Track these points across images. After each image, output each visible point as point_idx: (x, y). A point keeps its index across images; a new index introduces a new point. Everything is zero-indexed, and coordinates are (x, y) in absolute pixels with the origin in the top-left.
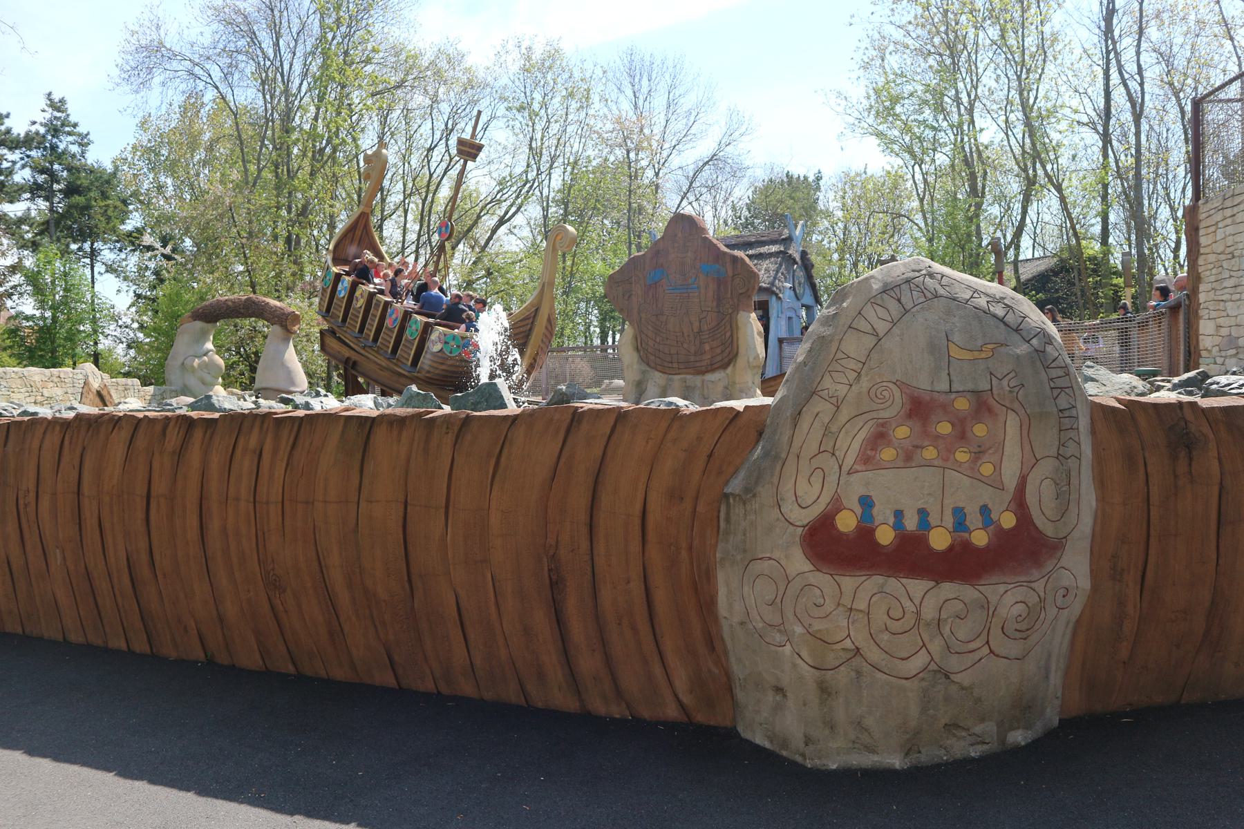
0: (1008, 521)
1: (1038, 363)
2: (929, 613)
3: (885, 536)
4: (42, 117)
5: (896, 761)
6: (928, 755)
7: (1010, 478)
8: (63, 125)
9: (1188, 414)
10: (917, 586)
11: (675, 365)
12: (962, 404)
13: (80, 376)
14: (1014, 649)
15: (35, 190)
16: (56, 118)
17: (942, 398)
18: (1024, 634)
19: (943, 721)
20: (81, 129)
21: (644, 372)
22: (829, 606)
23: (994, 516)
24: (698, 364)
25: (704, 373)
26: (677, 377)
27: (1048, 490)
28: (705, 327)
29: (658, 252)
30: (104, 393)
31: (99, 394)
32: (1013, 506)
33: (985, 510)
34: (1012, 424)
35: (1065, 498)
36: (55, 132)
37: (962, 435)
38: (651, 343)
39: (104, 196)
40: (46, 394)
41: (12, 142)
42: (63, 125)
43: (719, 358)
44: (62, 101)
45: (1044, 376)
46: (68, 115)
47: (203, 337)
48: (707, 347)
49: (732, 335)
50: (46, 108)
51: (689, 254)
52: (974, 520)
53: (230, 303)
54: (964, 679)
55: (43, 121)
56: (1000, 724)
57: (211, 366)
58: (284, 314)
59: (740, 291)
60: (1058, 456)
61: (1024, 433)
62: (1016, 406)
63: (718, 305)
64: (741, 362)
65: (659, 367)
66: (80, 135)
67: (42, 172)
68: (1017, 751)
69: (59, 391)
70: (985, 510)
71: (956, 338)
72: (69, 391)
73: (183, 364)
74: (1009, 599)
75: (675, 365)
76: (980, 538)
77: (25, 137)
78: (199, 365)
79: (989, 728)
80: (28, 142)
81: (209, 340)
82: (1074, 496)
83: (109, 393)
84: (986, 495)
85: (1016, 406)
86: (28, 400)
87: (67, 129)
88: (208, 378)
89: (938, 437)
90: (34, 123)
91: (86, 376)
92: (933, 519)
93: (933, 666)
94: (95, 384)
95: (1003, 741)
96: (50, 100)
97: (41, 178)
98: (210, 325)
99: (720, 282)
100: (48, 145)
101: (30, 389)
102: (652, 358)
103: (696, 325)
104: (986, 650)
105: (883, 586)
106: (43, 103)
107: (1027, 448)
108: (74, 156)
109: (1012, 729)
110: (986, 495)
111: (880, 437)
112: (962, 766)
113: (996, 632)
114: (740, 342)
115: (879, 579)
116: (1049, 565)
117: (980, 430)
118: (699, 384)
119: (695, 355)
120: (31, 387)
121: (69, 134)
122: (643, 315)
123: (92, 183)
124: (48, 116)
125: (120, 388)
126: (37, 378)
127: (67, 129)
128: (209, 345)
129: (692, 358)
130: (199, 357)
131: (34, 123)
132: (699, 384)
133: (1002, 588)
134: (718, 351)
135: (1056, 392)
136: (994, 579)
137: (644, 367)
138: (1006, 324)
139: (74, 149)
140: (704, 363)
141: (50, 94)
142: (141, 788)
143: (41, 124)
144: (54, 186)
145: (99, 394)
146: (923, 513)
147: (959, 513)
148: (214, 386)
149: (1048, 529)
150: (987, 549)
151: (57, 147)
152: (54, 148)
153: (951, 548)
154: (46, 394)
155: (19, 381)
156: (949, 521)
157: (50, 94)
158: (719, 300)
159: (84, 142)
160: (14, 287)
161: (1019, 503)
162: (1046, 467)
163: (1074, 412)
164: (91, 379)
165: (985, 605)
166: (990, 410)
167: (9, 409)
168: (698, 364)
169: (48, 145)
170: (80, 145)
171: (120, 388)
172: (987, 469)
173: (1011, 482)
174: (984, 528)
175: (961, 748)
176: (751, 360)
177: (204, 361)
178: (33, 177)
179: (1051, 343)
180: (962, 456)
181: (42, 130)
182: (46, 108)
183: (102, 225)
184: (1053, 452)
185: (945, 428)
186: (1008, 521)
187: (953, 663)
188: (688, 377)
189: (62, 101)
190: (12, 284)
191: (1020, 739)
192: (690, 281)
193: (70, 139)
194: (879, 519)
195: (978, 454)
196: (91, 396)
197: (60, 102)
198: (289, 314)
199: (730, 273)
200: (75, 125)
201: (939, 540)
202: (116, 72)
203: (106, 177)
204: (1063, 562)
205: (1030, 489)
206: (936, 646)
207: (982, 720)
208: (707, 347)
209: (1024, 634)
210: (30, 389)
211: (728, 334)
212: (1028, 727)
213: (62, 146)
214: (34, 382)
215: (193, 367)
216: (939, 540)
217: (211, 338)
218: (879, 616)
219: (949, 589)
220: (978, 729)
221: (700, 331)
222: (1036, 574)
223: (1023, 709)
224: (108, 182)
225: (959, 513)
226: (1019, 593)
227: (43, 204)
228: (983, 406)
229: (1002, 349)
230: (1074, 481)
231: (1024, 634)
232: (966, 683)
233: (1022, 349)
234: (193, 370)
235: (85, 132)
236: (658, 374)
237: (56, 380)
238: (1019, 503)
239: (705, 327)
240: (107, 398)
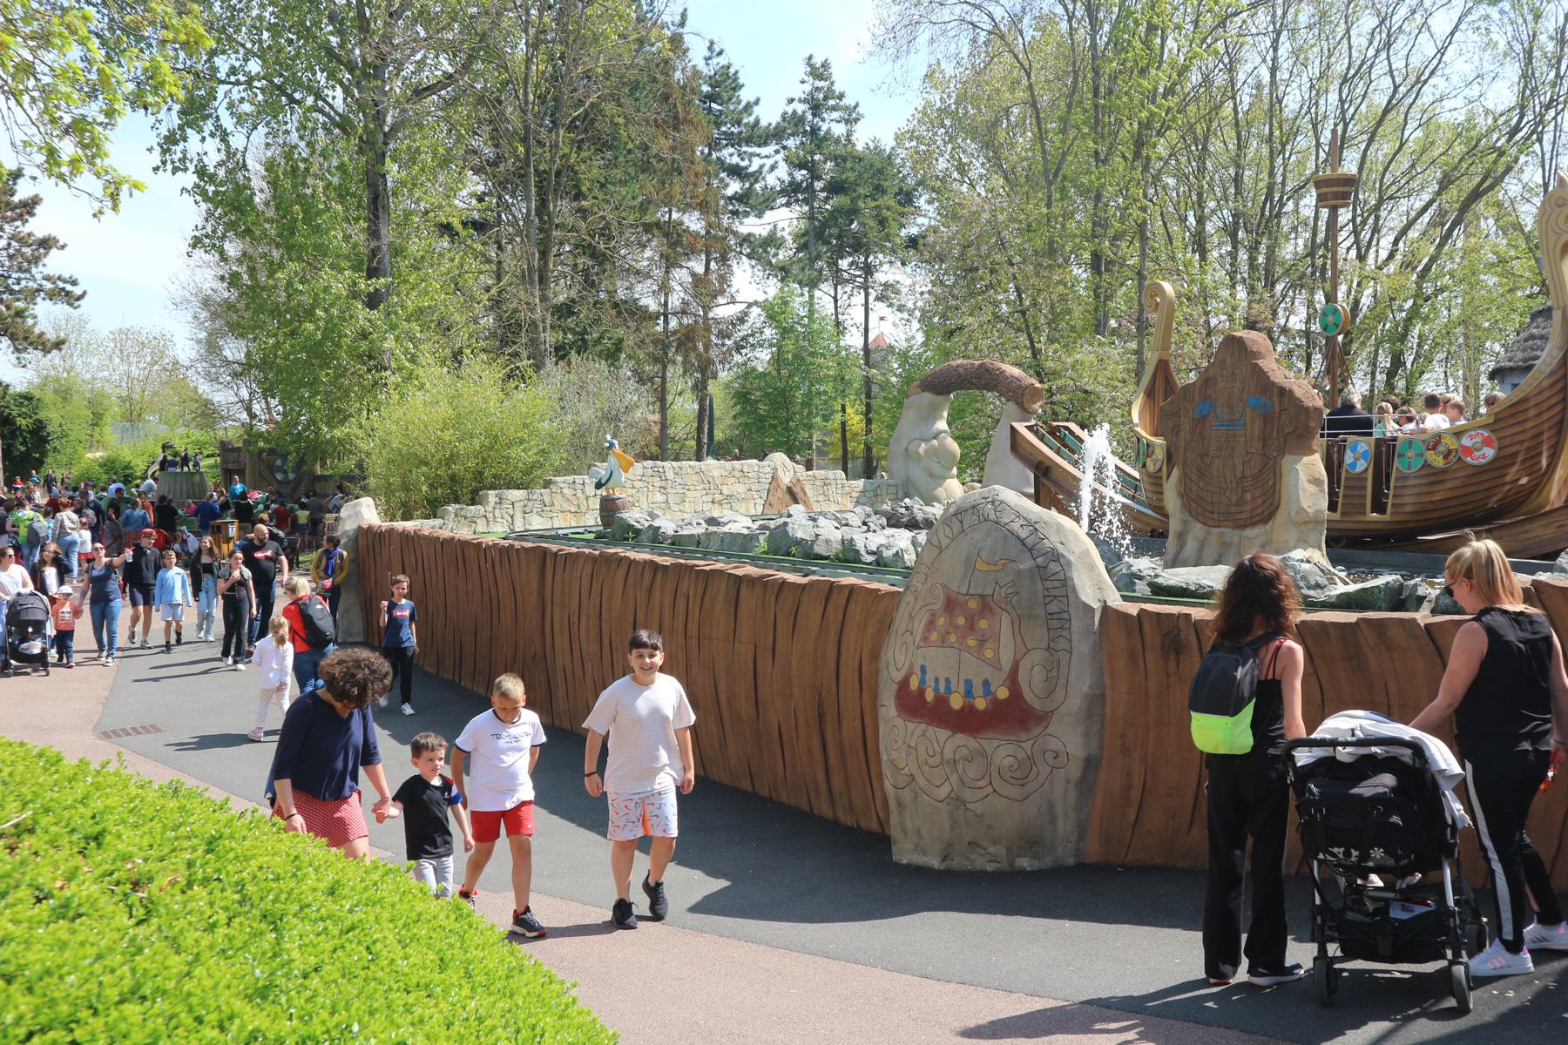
0: (1003, 693)
1: (1037, 577)
2: (948, 755)
3: (930, 696)
4: (800, 91)
5: (935, 863)
6: (957, 863)
7: (1006, 663)
8: (826, 98)
9: (1182, 624)
10: (943, 734)
11: (1215, 516)
12: (973, 604)
13: (768, 470)
14: (1014, 792)
15: (792, 191)
16: (818, 89)
17: (961, 599)
18: (1022, 782)
19: (968, 839)
20: (848, 101)
21: (1185, 523)
22: (900, 743)
23: (993, 689)
24: (1238, 516)
25: (1243, 527)
26: (1216, 530)
27: (1039, 674)
28: (1248, 473)
29: (1207, 380)
30: (796, 490)
31: (790, 491)
32: (1007, 683)
33: (986, 684)
34: (1006, 620)
35: (1052, 678)
36: (816, 108)
37: (971, 627)
38: (1194, 489)
39: (879, 189)
40: (726, 492)
41: (760, 137)
42: (826, 98)
43: (1259, 510)
44: (825, 65)
45: (1039, 586)
46: (832, 83)
47: (933, 414)
48: (1248, 497)
49: (1274, 484)
50: (806, 78)
51: (1237, 384)
52: (978, 689)
53: (961, 370)
54: (978, 808)
55: (803, 96)
56: (1009, 850)
57: (940, 454)
58: (1020, 387)
59: (1287, 430)
60: (1049, 648)
61: (1016, 629)
62: (1009, 608)
63: (1263, 446)
64: (1280, 516)
65: (1200, 518)
66: (847, 108)
67: (801, 166)
68: (1023, 873)
69: (741, 488)
70: (986, 684)
71: (983, 554)
72: (753, 488)
73: (907, 450)
74: (1002, 752)
75: (1215, 516)
76: (981, 704)
77: (775, 128)
78: (926, 451)
79: (999, 850)
80: (775, 135)
81: (942, 417)
82: (1062, 680)
83: (803, 489)
84: (988, 672)
85: (1009, 608)
86: (705, 499)
87: (832, 102)
88: (938, 470)
89: (957, 626)
90: (791, 101)
91: (775, 469)
92: (953, 687)
93: (953, 795)
94: (786, 479)
95: (1012, 864)
96: (811, 66)
97: (800, 175)
98: (940, 398)
99: (1267, 419)
100: (808, 128)
101: (707, 486)
102: (1194, 506)
103: (1239, 468)
104: (989, 789)
105: (925, 731)
106: (801, 70)
107: (1019, 640)
108: (837, 141)
109: (1019, 856)
110: (988, 672)
111: (931, 624)
112: (984, 873)
113: (995, 776)
114: (1283, 493)
115: (923, 726)
116: (1036, 731)
117: (983, 624)
118: (1236, 540)
119: (1237, 505)
120: (708, 483)
121: (834, 108)
122: (1189, 455)
123: (860, 176)
124: (807, 88)
125: (818, 483)
126: (716, 473)
127: (832, 102)
128: (942, 425)
129: (1233, 509)
130: (926, 440)
131: (791, 101)
132: (1236, 540)
133: (996, 743)
134: (1260, 501)
135: (1047, 600)
136: (989, 735)
137: (1187, 516)
138: (1024, 545)
139: (839, 130)
140: (1243, 516)
141: (810, 58)
142: (555, 818)
143: (800, 101)
144: (816, 184)
145: (790, 491)
146: (947, 680)
147: (968, 683)
148: (945, 479)
149: (1036, 704)
150: (984, 712)
151: (819, 129)
152: (815, 130)
153: (963, 708)
154: (726, 492)
155: (696, 477)
156: (962, 688)
157: (810, 58)
158: (1265, 440)
159: (851, 117)
160: (744, 338)
161: (1013, 681)
162: (1037, 656)
163: (1066, 616)
164: (780, 473)
165: (984, 754)
166: (991, 610)
167: (641, 521)
168: (1238, 516)
169: (808, 128)
170: (847, 122)
171: (818, 483)
172: (989, 654)
173: (1007, 665)
174: (984, 697)
175: (980, 863)
176: (1292, 514)
177: (933, 446)
178: (790, 174)
179: (1058, 560)
180: (971, 642)
181: (800, 108)
182: (806, 78)
183: (874, 235)
184: (1044, 644)
185: (961, 621)
186: (1003, 693)
187: (967, 795)
188: (1228, 530)
189: (825, 65)
190: (741, 334)
191: (1025, 865)
192: (1238, 416)
193: (835, 115)
194: (928, 684)
195: (982, 642)
196: (780, 494)
197: (823, 66)
198: (1026, 388)
199: (1277, 408)
200: (841, 97)
201: (956, 702)
202: (866, 39)
203: (878, 165)
204: (1050, 730)
205: (1021, 671)
206: (954, 779)
207: (995, 843)
208: (1248, 497)
209: (1021, 782)
210: (707, 486)
211: (1271, 483)
212: (1035, 857)
213: (824, 127)
214: (713, 477)
215: (918, 453)
216: (956, 702)
217: (945, 414)
218: (922, 751)
219: (961, 738)
220: (992, 850)
221: (1243, 477)
222: (1023, 736)
223: (1030, 842)
224: (881, 172)
225: (968, 683)
226: (1011, 749)
227: (799, 210)
228: (986, 606)
229: (1011, 565)
230: (1064, 669)
231: (1021, 782)
232: (979, 812)
233: (1026, 564)
234: (918, 457)
235: (853, 104)
236: (1198, 526)
237: (738, 474)
238: (1013, 681)
239: (1248, 473)
240: (800, 495)
